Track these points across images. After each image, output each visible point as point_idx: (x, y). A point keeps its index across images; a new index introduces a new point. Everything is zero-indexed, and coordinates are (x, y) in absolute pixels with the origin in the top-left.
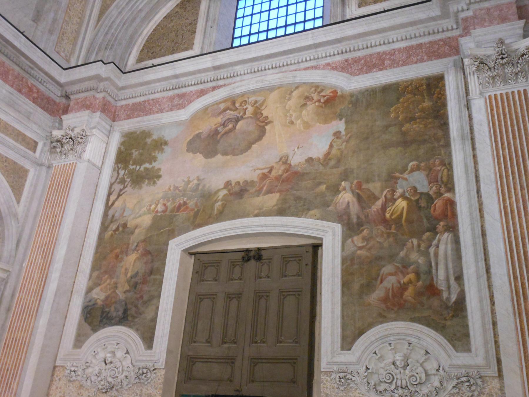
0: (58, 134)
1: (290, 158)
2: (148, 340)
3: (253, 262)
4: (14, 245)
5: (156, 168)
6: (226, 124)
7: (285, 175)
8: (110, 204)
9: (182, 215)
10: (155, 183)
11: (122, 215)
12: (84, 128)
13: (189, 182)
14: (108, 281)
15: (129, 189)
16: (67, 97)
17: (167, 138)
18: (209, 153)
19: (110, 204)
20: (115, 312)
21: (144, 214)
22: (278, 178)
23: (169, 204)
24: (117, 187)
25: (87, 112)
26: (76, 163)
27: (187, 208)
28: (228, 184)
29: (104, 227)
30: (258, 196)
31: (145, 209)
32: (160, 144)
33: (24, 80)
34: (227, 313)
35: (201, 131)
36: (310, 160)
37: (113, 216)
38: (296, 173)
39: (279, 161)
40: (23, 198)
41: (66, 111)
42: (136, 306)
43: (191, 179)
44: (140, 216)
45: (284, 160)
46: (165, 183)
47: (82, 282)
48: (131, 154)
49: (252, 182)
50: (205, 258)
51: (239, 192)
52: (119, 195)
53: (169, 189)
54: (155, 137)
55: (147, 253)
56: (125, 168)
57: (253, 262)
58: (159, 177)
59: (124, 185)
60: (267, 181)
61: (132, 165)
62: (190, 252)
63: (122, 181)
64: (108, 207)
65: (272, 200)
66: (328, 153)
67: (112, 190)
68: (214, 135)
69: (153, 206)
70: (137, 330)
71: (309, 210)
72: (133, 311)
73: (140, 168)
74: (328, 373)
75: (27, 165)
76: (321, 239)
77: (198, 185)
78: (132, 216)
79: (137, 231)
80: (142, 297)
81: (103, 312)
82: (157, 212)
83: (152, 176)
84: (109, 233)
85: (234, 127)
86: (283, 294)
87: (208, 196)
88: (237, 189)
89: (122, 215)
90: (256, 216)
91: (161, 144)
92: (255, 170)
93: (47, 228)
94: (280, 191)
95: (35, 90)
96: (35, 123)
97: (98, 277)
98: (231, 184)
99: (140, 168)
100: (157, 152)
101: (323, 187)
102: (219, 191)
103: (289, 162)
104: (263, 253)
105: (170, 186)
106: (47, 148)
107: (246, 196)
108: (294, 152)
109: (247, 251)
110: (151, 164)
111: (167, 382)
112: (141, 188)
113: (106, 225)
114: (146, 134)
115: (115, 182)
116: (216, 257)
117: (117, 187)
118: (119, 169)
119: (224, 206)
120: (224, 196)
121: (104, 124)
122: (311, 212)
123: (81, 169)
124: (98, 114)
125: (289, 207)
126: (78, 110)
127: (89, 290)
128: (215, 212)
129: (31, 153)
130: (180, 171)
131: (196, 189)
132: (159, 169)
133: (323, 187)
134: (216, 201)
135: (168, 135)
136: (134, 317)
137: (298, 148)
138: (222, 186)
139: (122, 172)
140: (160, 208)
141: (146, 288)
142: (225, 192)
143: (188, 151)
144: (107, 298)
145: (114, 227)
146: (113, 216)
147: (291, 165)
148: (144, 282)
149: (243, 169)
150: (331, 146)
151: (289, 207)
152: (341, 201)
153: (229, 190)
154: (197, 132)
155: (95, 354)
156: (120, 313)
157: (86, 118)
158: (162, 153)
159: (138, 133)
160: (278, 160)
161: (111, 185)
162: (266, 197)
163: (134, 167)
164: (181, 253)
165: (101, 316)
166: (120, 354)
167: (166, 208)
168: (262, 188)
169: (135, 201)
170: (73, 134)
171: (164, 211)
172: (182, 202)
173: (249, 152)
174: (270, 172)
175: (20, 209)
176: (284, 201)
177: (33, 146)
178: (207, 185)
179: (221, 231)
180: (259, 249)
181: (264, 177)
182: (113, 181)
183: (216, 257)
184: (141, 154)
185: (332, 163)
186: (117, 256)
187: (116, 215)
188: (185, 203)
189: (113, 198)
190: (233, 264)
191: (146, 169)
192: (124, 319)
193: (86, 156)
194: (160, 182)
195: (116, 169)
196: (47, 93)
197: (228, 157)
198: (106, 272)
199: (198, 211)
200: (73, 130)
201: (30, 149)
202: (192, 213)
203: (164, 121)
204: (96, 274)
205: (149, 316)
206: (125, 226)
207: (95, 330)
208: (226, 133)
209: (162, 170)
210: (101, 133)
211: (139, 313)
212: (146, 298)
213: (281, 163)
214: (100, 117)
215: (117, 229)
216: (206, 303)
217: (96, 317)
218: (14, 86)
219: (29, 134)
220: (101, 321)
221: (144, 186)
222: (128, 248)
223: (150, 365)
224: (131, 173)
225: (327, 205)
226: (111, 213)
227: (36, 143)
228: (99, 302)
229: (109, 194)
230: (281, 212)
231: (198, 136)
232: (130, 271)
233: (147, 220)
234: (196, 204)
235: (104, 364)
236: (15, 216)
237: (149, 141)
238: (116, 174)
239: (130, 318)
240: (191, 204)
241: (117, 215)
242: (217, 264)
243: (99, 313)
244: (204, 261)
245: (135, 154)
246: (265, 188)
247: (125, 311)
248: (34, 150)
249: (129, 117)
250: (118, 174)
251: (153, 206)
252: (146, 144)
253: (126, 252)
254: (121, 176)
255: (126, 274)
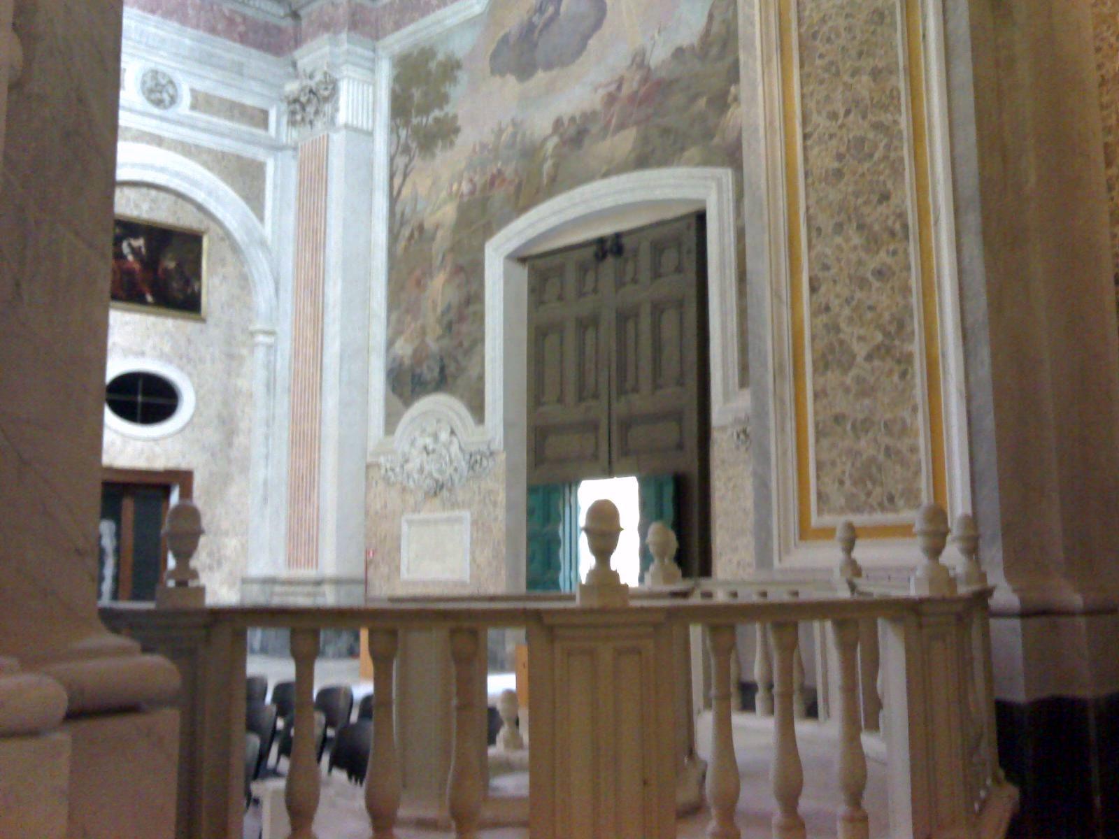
0: (292, 87)
1: (648, 54)
2: (478, 409)
3: (610, 260)
4: (272, 291)
5: (451, 115)
6: (543, 8)
7: (643, 90)
8: (395, 193)
9: (499, 194)
10: (452, 143)
11: (414, 210)
12: (325, 69)
13: (501, 131)
14: (413, 325)
15: (417, 162)
16: (295, 15)
17: (460, 54)
18: (524, 71)
19: (395, 193)
20: (429, 372)
21: (445, 202)
22: (632, 98)
23: (477, 178)
24: (401, 161)
25: (326, 36)
26: (328, 136)
27: (504, 180)
28: (558, 123)
29: (393, 236)
30: (604, 138)
31: (443, 194)
32: (451, 68)
33: (215, 7)
34: (581, 352)
35: (507, 30)
36: (679, 52)
37: (403, 214)
38: (659, 83)
39: (632, 64)
40: (268, 213)
41: (298, 42)
42: (456, 361)
43: (503, 126)
44: (439, 208)
45: (639, 60)
46: (468, 139)
47: (379, 332)
48: (410, 97)
49: (594, 113)
50: (539, 263)
51: (575, 135)
52: (405, 176)
53: (474, 150)
54: (441, 57)
55: (458, 269)
56: (407, 123)
57: (610, 260)
58: (456, 131)
59: (410, 155)
60: (616, 108)
61: (416, 117)
62: (521, 258)
63: (406, 150)
64: (393, 199)
65: (624, 142)
66: (707, 31)
67: (394, 169)
68: (529, 33)
69: (455, 187)
70: (461, 397)
71: (683, 149)
72: (452, 368)
73: (427, 120)
74: (723, 428)
75: (260, 154)
76: (704, 202)
77: (514, 135)
78: (428, 210)
79: (440, 234)
80: (461, 344)
81: (413, 376)
82: (462, 195)
83: (446, 132)
84: (402, 244)
85: (557, 12)
86: (658, 309)
87: (530, 152)
88: (572, 131)
89: (414, 210)
90: (606, 175)
91: (452, 69)
92: (596, 89)
93: (308, 256)
94: (638, 123)
95: (239, 20)
96: (254, 78)
97: (399, 321)
98: (563, 124)
99: (427, 120)
100: (447, 84)
101: (702, 102)
102: (545, 139)
103: (646, 62)
104: (626, 241)
105: (475, 146)
106: (285, 119)
107: (587, 141)
108: (652, 42)
109: (601, 241)
110: (441, 108)
111: (511, 469)
112: (433, 156)
113: (395, 231)
114: (426, 54)
115: (396, 152)
116: (558, 259)
117: (401, 161)
118: (398, 127)
119: (556, 166)
120: (556, 147)
121: (360, 50)
122: (687, 154)
123: (338, 140)
124: (344, 36)
125: (653, 151)
126: (314, 35)
127: (390, 343)
128: (545, 180)
129: (259, 132)
130: (488, 111)
131: (512, 145)
132: (455, 117)
133: (702, 102)
134: (545, 159)
135: (461, 46)
136: (455, 378)
137: (659, 32)
138: (549, 130)
139: (403, 133)
140: (465, 187)
141: (465, 328)
142: (555, 140)
143: (493, 72)
144: (415, 352)
145: (406, 232)
146: (403, 214)
147: (649, 69)
148: (461, 318)
149: (577, 91)
150: (711, 17)
151: (653, 151)
152: (731, 123)
153: (561, 136)
154: (502, 34)
155: (413, 443)
156: (436, 373)
157: (327, 49)
158: (455, 86)
159: (415, 53)
160: (629, 62)
161: (392, 160)
162: (617, 138)
163: (419, 119)
164: (504, 264)
165: (412, 383)
166: (444, 436)
167: (474, 185)
168: (610, 121)
169: (429, 182)
170: (312, 84)
171: (472, 192)
172: (495, 171)
173: (585, 53)
174: (619, 88)
175: (268, 230)
176: (645, 139)
177: (260, 119)
178: (528, 133)
179: (554, 213)
180: (618, 236)
181: (611, 99)
182: (393, 151)
183: (558, 259)
184: (426, 94)
185: (714, 51)
186: (418, 283)
187: (406, 213)
188: (500, 172)
189: (397, 181)
190: (583, 269)
191: (437, 120)
192: (442, 382)
193: (342, 118)
194: (460, 140)
195: (394, 130)
196: (260, 17)
197: (554, 72)
198: (407, 311)
199: (520, 185)
200: (311, 77)
201: (256, 125)
202: (512, 189)
203: (450, 22)
204: (394, 317)
205: (474, 373)
206: (421, 228)
207: (408, 403)
208: (547, 25)
209: (460, 117)
210: (359, 70)
211: (461, 370)
212: (466, 344)
213: (634, 67)
214: (349, 42)
215: (411, 236)
216: (553, 339)
217: (407, 383)
218: (202, 25)
219: (249, 101)
220: (413, 391)
221: (438, 151)
222: (431, 266)
223: (484, 448)
224: (416, 131)
225: (708, 134)
226: (398, 209)
227: (265, 114)
228: (407, 362)
229: (392, 177)
230: (642, 161)
231: (505, 40)
232: (439, 303)
233: (448, 213)
234: (516, 171)
235: (425, 455)
236: (263, 243)
237: (433, 65)
238: (395, 136)
239: (449, 379)
240: (509, 172)
241: (408, 211)
242: (560, 270)
243: (409, 379)
244: (542, 269)
245: (417, 93)
246: (614, 121)
247: (442, 369)
248: (264, 123)
249: (398, 26)
250: (399, 137)
251: (455, 187)
252: (429, 73)
253: (428, 273)
254: (402, 140)
255: (434, 309)
